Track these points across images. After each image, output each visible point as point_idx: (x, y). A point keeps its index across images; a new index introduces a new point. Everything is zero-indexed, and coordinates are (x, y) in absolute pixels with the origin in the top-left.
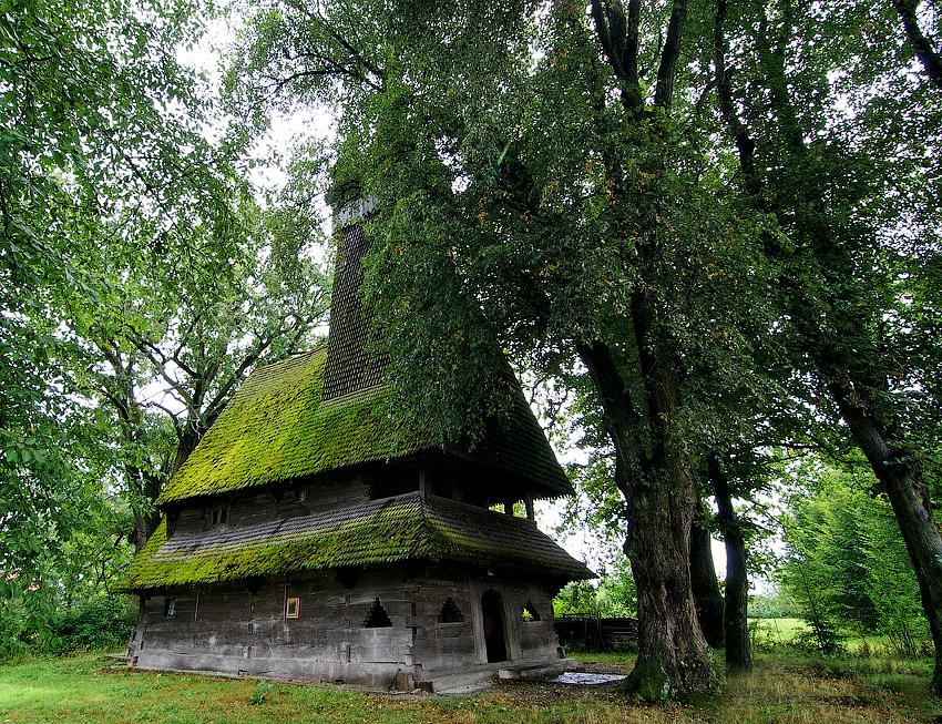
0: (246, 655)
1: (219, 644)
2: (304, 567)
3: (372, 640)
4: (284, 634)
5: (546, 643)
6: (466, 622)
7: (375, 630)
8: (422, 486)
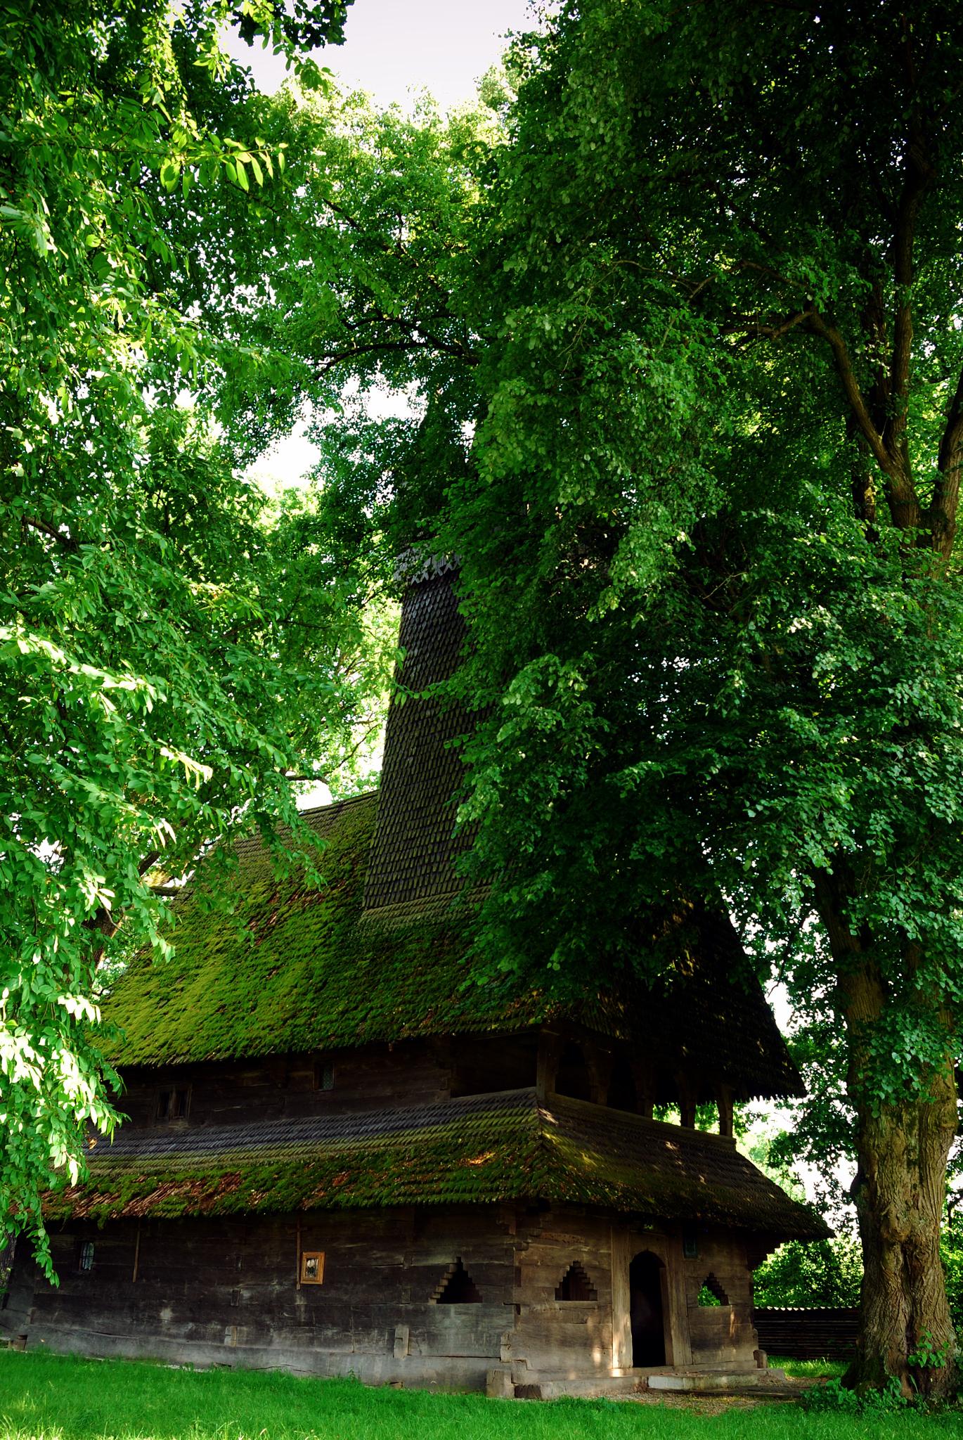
1: (177, 1321)
2: (337, 1204)
3: (447, 1322)
4: (294, 1310)
5: (736, 1341)
6: (601, 1301)
7: (453, 1308)
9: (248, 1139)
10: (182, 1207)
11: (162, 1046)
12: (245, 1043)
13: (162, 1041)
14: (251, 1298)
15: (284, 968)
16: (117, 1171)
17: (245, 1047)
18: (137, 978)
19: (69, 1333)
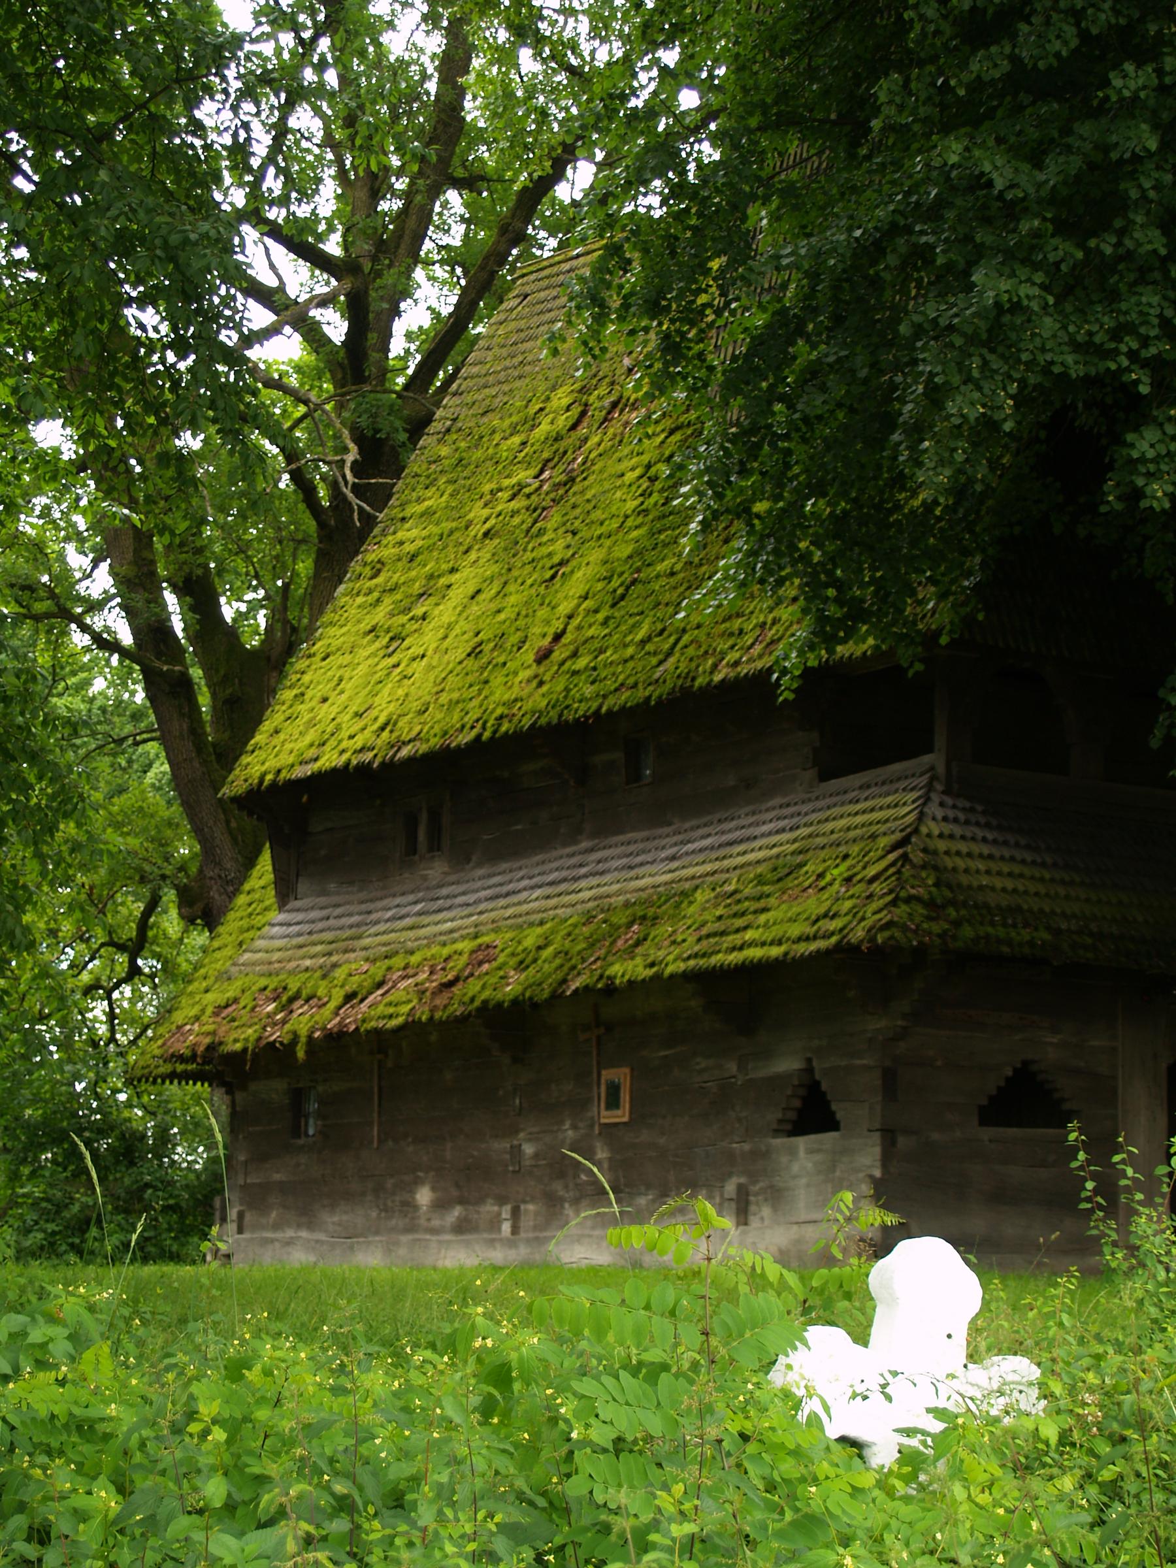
0: (506, 1227)
1: (440, 1205)
3: (795, 1168)
7: (802, 1143)
8: (940, 741)
9: (525, 883)
10: (405, 1009)
11: (383, 729)
12: (499, 711)
13: (382, 720)
14: (536, 1156)
15: (573, 563)
16: (334, 959)
17: (501, 717)
18: (360, 600)
19: (289, 1243)
